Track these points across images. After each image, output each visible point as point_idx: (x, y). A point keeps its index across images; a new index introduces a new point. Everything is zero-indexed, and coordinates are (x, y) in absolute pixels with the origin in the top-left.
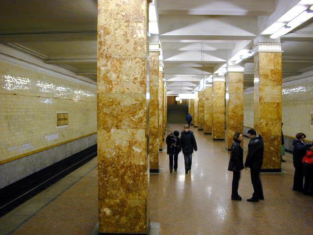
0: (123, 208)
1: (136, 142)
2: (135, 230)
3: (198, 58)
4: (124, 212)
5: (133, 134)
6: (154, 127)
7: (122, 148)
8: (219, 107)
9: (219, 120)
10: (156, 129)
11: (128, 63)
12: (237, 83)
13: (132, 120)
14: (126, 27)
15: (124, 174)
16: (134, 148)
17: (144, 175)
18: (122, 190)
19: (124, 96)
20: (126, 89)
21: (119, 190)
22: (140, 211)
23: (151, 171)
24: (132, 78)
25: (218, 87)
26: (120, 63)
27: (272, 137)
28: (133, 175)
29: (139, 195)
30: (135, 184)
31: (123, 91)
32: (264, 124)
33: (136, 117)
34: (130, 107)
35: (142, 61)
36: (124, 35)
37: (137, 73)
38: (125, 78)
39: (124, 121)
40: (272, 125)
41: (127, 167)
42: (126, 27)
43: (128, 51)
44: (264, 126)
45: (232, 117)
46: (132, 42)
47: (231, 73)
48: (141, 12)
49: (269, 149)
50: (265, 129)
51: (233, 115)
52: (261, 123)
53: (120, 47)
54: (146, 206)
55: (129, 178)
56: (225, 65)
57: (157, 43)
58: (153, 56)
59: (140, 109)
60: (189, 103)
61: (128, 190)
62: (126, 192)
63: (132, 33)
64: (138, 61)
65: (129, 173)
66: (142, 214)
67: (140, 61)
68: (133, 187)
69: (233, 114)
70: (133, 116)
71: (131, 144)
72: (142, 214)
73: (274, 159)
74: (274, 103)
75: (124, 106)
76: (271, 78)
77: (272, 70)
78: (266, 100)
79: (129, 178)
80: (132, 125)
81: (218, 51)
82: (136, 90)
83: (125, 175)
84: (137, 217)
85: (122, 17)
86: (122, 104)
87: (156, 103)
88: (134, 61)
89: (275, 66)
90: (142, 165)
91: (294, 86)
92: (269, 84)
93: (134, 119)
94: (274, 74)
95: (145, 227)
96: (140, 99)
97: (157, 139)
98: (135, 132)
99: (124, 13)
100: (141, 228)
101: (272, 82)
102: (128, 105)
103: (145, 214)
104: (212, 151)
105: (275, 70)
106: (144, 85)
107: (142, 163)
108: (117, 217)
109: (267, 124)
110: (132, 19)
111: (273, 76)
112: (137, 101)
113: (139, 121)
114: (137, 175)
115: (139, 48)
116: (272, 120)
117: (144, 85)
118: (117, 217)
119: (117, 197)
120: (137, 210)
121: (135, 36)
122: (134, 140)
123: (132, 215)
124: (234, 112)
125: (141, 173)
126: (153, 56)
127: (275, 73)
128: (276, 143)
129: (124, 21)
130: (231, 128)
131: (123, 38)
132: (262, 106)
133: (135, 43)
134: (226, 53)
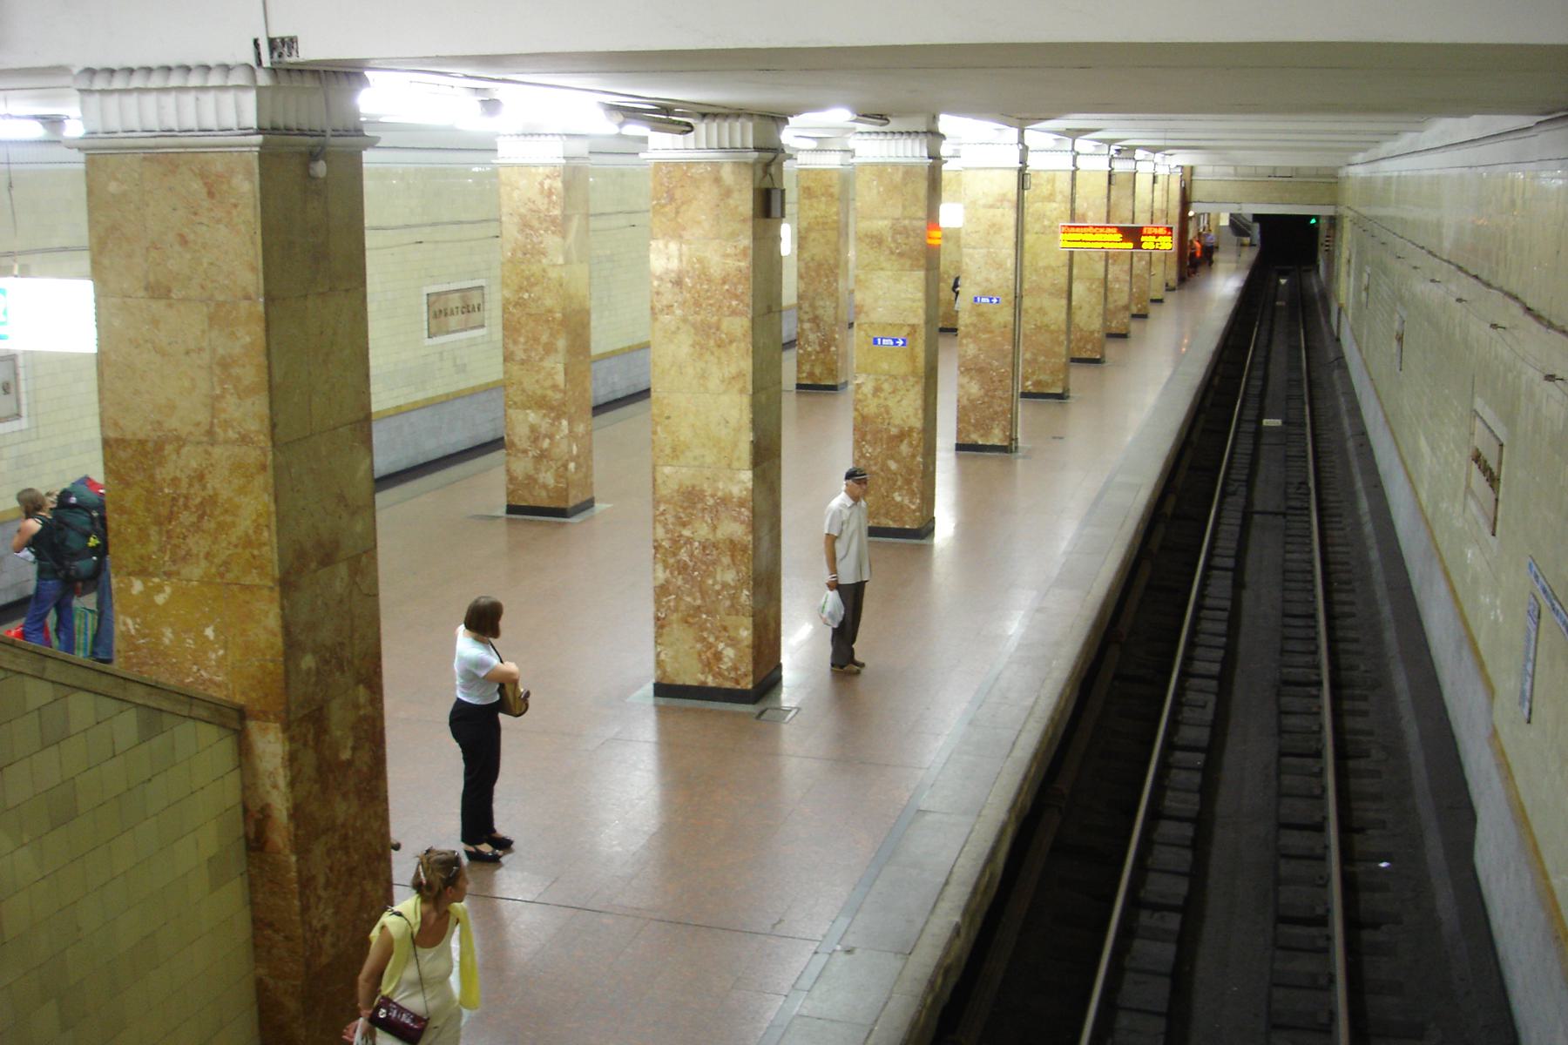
6: (555, 387)
8: (1046, 268)
9: (1046, 320)
12: (991, 207)
27: (894, 431)
49: (885, 468)
51: (974, 325)
69: (974, 319)
73: (898, 499)
74: (901, 326)
89: (904, 207)
92: (884, 265)
109: (877, 390)
111: (900, 239)
124: (980, 315)
128: (904, 448)
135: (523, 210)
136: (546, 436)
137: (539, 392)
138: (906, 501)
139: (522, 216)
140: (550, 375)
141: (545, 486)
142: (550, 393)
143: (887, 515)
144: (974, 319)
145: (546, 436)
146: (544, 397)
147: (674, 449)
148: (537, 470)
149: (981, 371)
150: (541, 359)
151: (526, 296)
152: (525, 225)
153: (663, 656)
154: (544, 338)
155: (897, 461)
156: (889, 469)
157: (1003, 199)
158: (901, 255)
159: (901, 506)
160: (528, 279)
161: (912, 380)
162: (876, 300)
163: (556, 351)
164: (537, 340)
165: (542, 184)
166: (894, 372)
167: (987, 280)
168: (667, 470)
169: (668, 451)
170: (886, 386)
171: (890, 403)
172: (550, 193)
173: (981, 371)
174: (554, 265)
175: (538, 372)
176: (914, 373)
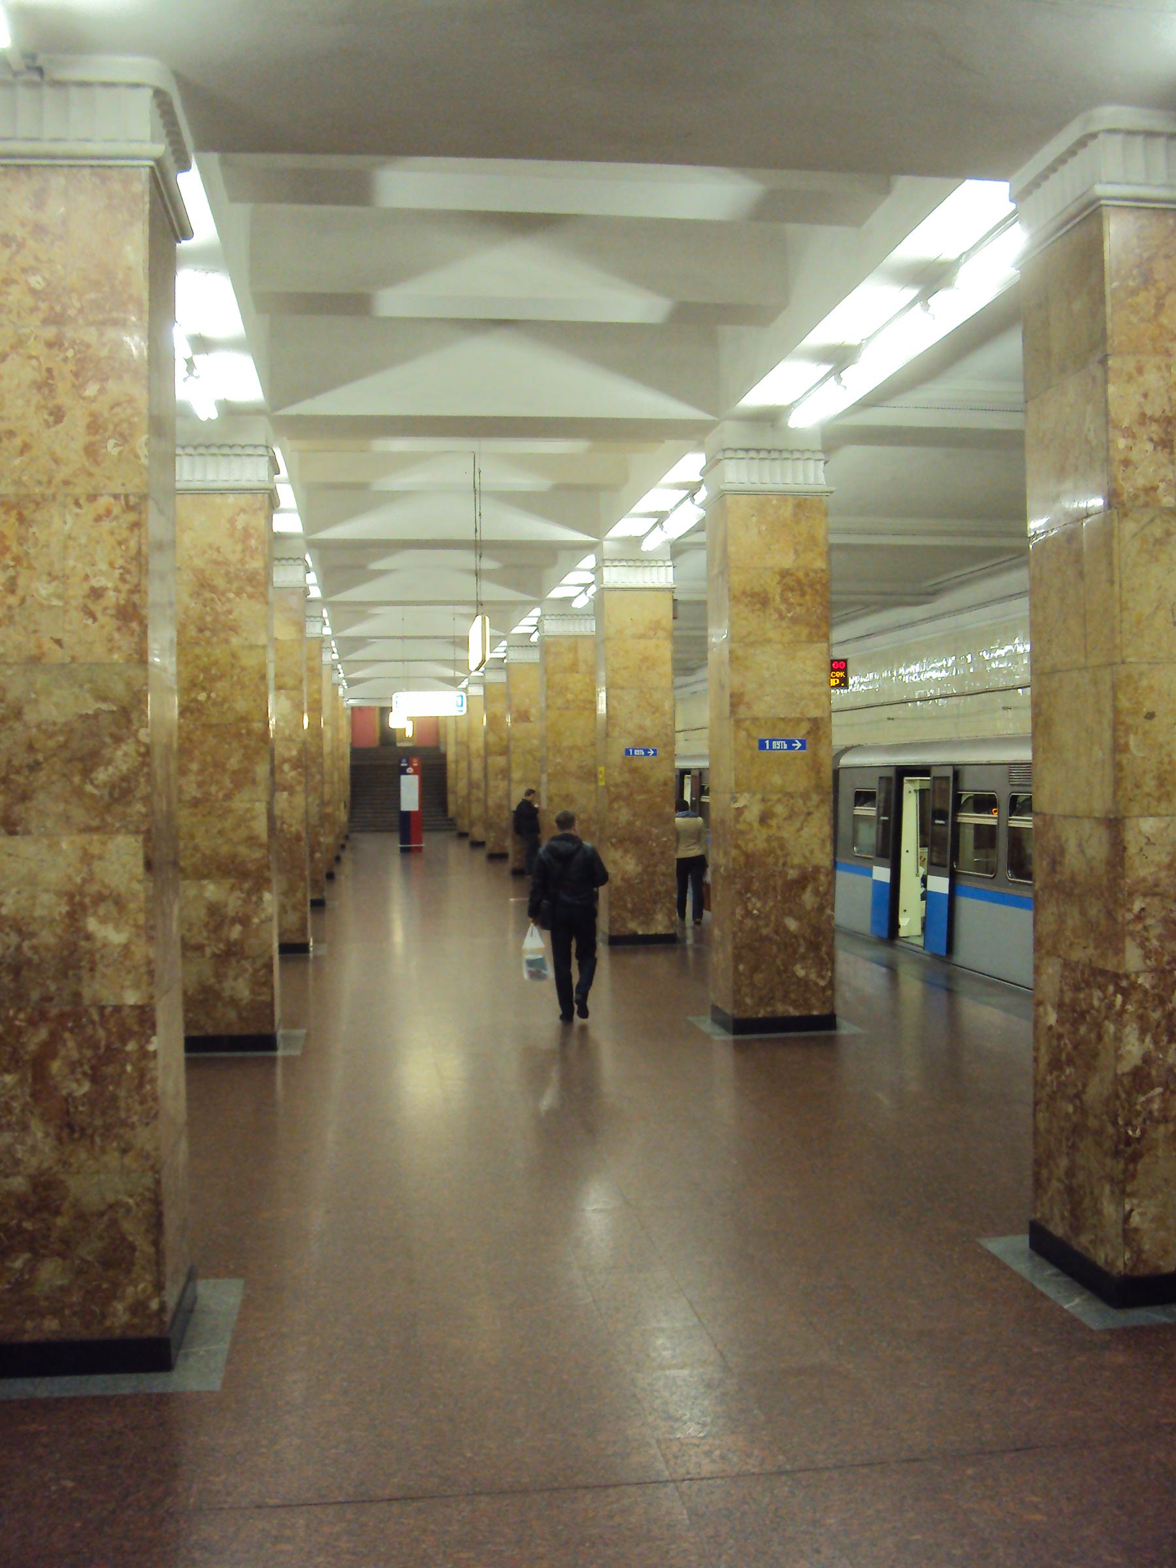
0: (45, 1215)
1: (100, 898)
2: (108, 1323)
3: (453, 518)
4: (54, 1235)
5: (87, 858)
6: (251, 840)
7: (34, 927)
8: (571, 748)
10: (261, 846)
11: (57, 523)
12: (642, 636)
13: (78, 792)
14: (50, 345)
15: (49, 1050)
16: (92, 924)
17: (145, 1055)
18: (38, 1132)
19: (41, 680)
20: (48, 645)
21: (25, 1128)
22: (127, 1226)
23: (199, 1045)
24: (78, 592)
25: (567, 660)
26: (21, 519)
27: (792, 874)
28: (89, 1053)
29: (124, 1151)
30: (102, 1102)
31: (35, 651)
32: (753, 814)
33: (102, 775)
34: (68, 729)
35: (129, 508)
36: (39, 386)
37: (103, 566)
38: (44, 590)
39: (41, 796)
40: (790, 817)
41: (62, 1016)
42: (50, 345)
43: (56, 461)
44: (756, 825)
45: (625, 791)
46: (77, 419)
47: (617, 593)
48: (121, 276)
49: (780, 928)
50: (758, 841)
51: (627, 784)
52: (740, 811)
53: (18, 442)
54: (157, 1202)
55: (73, 1072)
56: (590, 561)
57: (261, 451)
58: (242, 510)
59: (118, 740)
60: (451, 738)
61: (69, 1128)
62: (59, 1139)
63: (76, 375)
64: (108, 512)
65: (71, 1044)
66: (144, 1245)
67: (116, 510)
68: (92, 1114)
69: (627, 777)
70: (86, 773)
71: (78, 904)
72: (144, 1245)
73: (801, 973)
74: (798, 721)
75: (39, 726)
76: (783, 607)
77: (784, 574)
78: (761, 709)
79: (73, 1072)
80: (79, 815)
81: (561, 488)
82: (99, 650)
83: (54, 1056)
84: (118, 1257)
85: (29, 301)
86: (30, 716)
87: (257, 726)
88: (89, 511)
90: (133, 1007)
91: (907, 655)
92: (771, 634)
93: (89, 788)
94: (792, 590)
95: (154, 1305)
96: (119, 689)
97: (267, 896)
98: (95, 849)
99: (36, 281)
100: (138, 1308)
101: (784, 624)
102: (61, 720)
103: (156, 1243)
104: (337, 903)
105: (801, 574)
106: (134, 625)
107: (131, 998)
108: (18, 1264)
109: (764, 819)
110: (81, 311)
111: (792, 598)
112: (104, 699)
113: (116, 794)
114: (112, 1054)
115: (111, 448)
116: (791, 795)
117: (134, 625)
118: (18, 1264)
119: (17, 1162)
120: (114, 1223)
121: (91, 390)
122: (93, 888)
123: (88, 1250)
124: (633, 771)
125: (131, 1046)
126: (242, 510)
127: (800, 588)
129: (35, 320)
130: (621, 841)
131: (36, 398)
132: (743, 734)
133: (94, 426)
134: (587, 502)
135: (198, 562)
136: (234, 921)
137: (225, 849)
138: (813, 976)
139: (198, 573)
140: (242, 821)
141: (234, 1002)
142: (243, 850)
143: (785, 998)
144: (627, 777)
145: (234, 921)
146: (234, 857)
147: (1161, 781)
148: (220, 976)
149: (637, 841)
150: (228, 797)
151: (202, 697)
152: (203, 585)
153: (1135, 1220)
154: (234, 763)
155: (799, 918)
156: (786, 930)
157: (656, 626)
158: (795, 621)
159: (804, 983)
160: (206, 670)
161: (815, 798)
162: (761, 686)
163: (254, 782)
164: (219, 766)
165: (232, 521)
166: (790, 789)
167: (641, 727)
168: (1148, 825)
169: (1149, 784)
170: (780, 809)
171: (785, 834)
172: (247, 534)
173: (637, 841)
174: (252, 647)
175: (222, 817)
176: (818, 787)
